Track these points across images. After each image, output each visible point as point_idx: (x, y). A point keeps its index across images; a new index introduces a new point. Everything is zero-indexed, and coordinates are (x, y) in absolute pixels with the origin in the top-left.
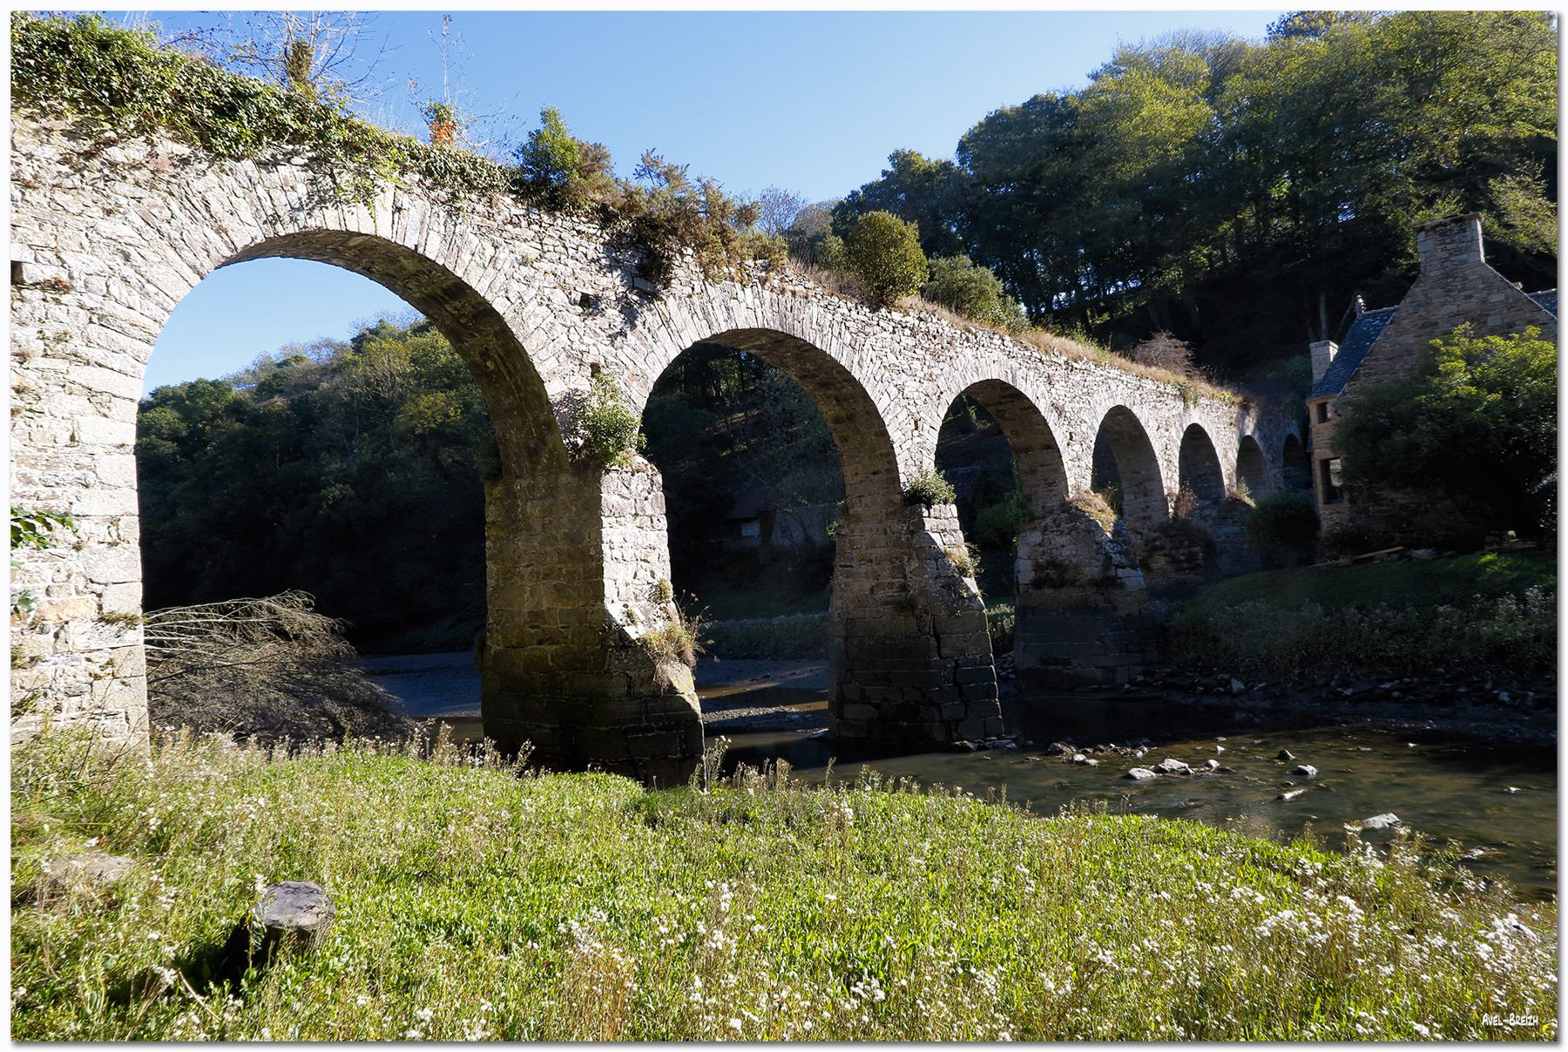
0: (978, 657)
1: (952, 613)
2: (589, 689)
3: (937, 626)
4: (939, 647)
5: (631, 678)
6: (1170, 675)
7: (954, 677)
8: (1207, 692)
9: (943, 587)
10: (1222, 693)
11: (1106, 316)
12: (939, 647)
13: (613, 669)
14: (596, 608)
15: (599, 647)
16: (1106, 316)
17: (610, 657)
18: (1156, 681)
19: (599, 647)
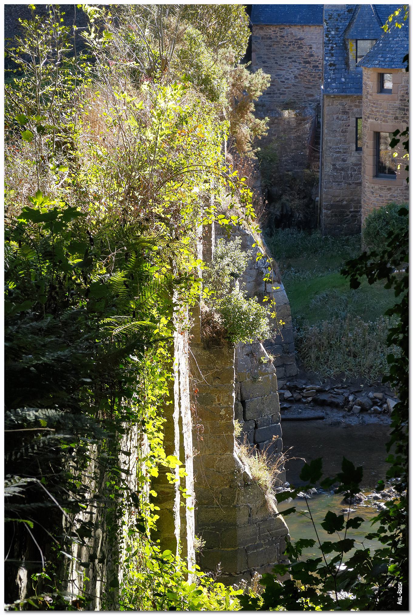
0: (270, 416)
1: (255, 379)
2: (216, 520)
3: (244, 394)
4: (244, 412)
5: (251, 509)
6: (319, 391)
7: (254, 436)
8: (364, 410)
9: (248, 355)
10: (380, 413)
11: (391, 20)
12: (244, 412)
13: (240, 504)
14: (223, 457)
15: (227, 487)
16: (391, 20)
17: (238, 494)
18: (306, 397)
19: (227, 487)
